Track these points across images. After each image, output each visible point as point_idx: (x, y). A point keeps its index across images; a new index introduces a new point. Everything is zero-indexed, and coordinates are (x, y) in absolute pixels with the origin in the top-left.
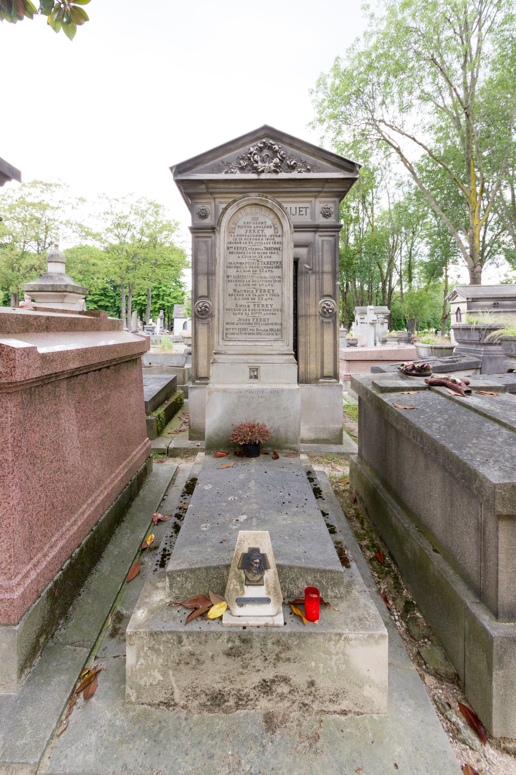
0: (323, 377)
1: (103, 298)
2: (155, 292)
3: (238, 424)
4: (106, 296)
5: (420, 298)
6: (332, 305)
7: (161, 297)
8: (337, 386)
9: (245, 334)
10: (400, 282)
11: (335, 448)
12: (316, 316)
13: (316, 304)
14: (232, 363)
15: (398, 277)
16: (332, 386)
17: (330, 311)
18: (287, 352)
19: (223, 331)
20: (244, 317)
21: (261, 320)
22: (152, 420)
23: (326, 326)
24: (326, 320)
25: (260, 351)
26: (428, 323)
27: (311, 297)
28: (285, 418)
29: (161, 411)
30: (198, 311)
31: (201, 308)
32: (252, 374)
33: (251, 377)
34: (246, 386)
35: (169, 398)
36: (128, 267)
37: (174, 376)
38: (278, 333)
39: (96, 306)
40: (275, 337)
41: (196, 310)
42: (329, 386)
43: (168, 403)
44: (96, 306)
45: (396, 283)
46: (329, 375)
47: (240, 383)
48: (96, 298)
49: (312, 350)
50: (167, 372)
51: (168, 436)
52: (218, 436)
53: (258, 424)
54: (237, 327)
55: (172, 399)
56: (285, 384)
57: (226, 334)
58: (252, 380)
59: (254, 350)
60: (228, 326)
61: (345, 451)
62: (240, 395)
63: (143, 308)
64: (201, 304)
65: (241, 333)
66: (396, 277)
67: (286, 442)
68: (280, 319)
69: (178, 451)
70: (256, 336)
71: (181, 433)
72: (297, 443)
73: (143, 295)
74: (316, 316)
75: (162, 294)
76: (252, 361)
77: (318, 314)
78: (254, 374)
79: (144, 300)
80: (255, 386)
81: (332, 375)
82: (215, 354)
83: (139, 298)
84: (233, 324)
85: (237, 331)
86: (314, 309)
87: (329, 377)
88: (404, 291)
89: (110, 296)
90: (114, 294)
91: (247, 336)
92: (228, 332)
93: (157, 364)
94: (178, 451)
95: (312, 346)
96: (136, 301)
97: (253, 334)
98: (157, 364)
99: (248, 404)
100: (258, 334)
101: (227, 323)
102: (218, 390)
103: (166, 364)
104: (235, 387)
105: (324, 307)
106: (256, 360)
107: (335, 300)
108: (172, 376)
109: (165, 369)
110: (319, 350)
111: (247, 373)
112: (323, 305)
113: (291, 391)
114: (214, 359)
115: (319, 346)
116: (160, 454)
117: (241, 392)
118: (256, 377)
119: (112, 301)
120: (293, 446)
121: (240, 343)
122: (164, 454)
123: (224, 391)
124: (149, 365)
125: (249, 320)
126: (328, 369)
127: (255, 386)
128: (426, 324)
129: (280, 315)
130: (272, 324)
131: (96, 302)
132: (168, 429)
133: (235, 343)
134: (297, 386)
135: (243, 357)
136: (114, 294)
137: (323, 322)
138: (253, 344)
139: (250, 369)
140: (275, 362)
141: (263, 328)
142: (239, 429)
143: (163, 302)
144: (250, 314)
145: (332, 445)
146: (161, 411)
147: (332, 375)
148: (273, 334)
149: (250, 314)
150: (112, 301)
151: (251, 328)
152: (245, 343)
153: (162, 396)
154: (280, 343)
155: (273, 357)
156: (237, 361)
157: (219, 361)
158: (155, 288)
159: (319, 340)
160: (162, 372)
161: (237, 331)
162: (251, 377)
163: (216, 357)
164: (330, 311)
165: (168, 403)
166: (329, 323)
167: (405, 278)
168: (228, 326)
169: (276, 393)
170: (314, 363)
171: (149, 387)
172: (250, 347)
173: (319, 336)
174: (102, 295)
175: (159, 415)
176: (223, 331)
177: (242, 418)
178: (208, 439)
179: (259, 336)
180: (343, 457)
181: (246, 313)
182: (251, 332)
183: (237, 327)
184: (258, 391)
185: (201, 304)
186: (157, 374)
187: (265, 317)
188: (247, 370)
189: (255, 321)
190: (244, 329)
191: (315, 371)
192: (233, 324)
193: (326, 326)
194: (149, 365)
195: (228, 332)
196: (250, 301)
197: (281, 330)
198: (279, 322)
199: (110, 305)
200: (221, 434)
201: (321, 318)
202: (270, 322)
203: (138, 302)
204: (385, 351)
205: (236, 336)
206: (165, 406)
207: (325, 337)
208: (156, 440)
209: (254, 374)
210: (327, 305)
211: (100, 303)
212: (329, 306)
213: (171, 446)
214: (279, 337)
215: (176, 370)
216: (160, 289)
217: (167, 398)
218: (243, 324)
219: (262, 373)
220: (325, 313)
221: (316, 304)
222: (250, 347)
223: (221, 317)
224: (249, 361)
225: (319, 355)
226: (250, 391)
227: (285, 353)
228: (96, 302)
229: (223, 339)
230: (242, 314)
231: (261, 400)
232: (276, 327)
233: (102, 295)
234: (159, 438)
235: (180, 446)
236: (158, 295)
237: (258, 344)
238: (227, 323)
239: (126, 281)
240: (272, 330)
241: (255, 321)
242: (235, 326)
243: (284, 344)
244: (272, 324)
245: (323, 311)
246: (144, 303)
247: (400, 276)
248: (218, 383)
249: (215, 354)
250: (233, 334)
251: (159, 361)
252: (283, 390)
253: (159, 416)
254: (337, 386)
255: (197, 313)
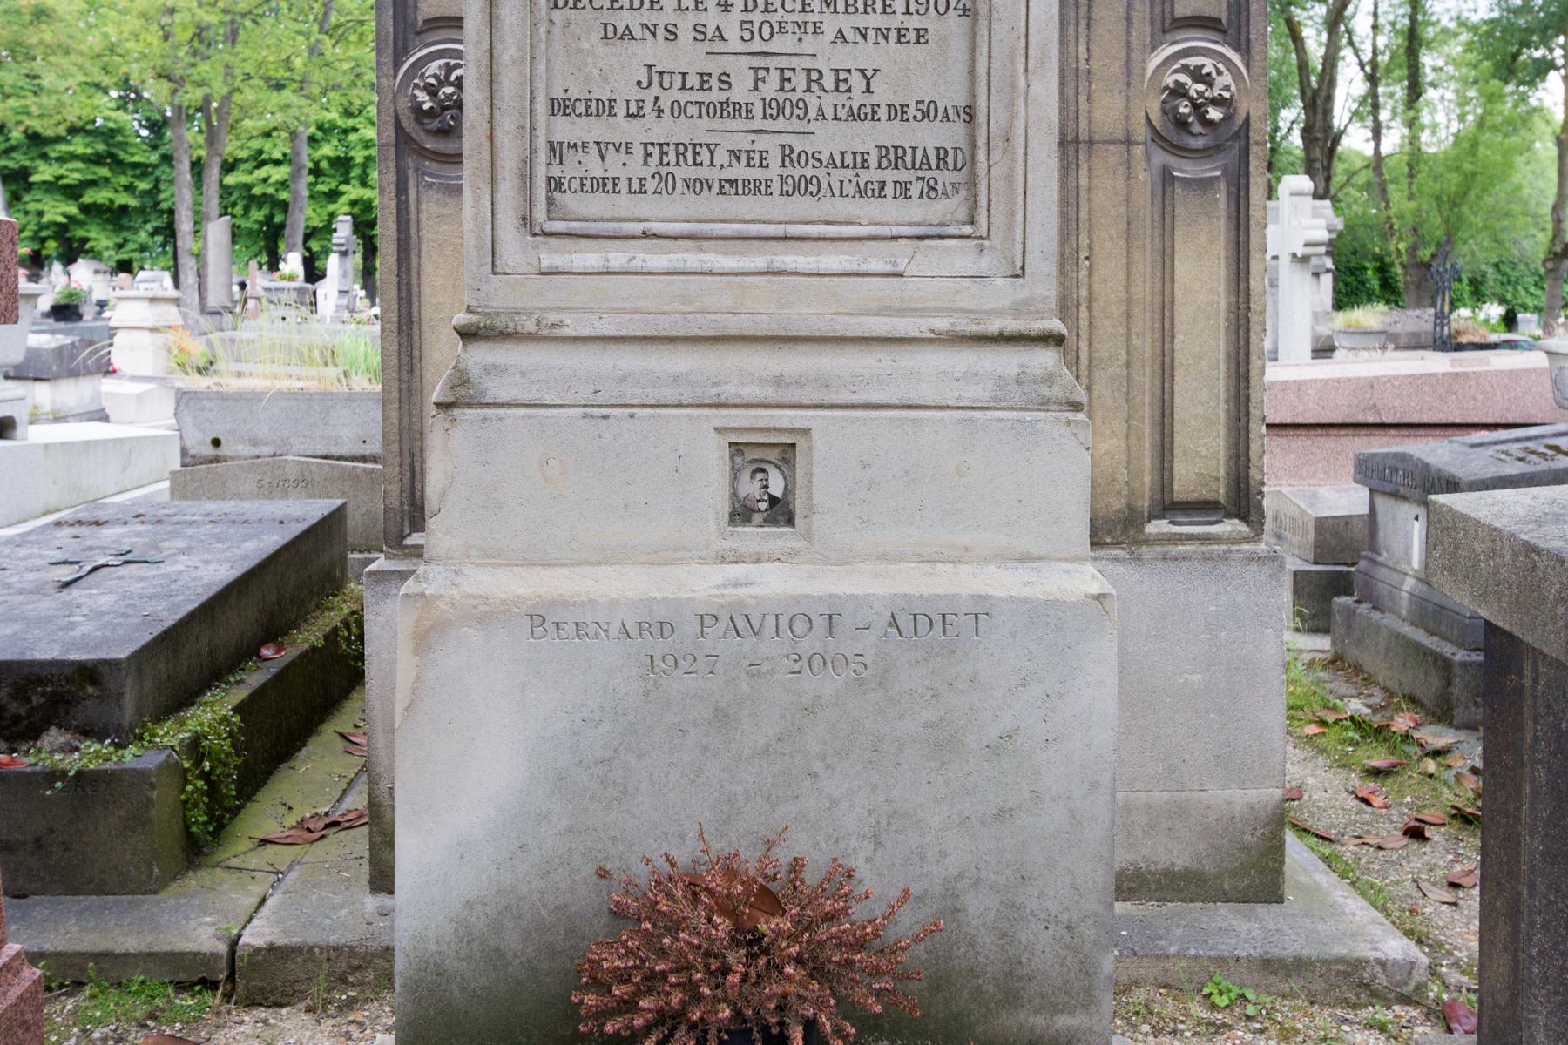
0: (1169, 507)
1: (104, 172)
2: (327, 150)
3: (642, 874)
4: (118, 164)
5: (1467, 167)
6: (1227, 79)
7: (355, 172)
8: (1253, 558)
9: (697, 186)
10: (1372, 103)
11: (1242, 930)
12: (1129, 142)
13: (1129, 70)
14: (597, 408)
15: (1360, 87)
16: (1224, 557)
17: (1214, 114)
18: (1012, 325)
19: (528, 162)
20: (687, 56)
21: (814, 79)
22: (140, 775)
23: (1185, 204)
24: (1186, 169)
25: (806, 313)
26: (1472, 282)
27: (1099, 30)
28: (1003, 814)
29: (213, 713)
30: (417, 109)
31: (432, 91)
32: (750, 488)
33: (741, 513)
34: (704, 584)
35: (293, 625)
36: (200, 33)
37: (339, 502)
38: (945, 177)
39: (73, 210)
40: (918, 210)
41: (404, 104)
42: (1206, 559)
43: (275, 658)
44: (73, 210)
45: (1347, 116)
46: (1204, 493)
47: (658, 557)
48: (73, 174)
49: (1103, 349)
50: (305, 484)
51: (253, 861)
52: (496, 957)
53: (797, 865)
54: (635, 132)
55: (308, 637)
56: (1002, 558)
57: (554, 185)
58: (754, 536)
59: (763, 308)
60: (566, 129)
61: (1309, 952)
62: (660, 647)
63: (278, 219)
64: (434, 67)
65: (666, 182)
66: (1349, 85)
67: (1011, 997)
68: (958, 71)
69: (294, 968)
70: (773, 210)
71: (334, 837)
72: (1087, 1001)
73: (277, 163)
74: (1129, 142)
75: (359, 156)
76: (749, 392)
77: (1141, 132)
78: (767, 495)
79: (283, 184)
80: (774, 575)
81: (1221, 494)
82: (468, 335)
83: (262, 173)
84: (605, 108)
85: (636, 168)
86: (1118, 103)
87: (1205, 508)
88: (1386, 148)
89: (135, 165)
90: (154, 158)
91: (711, 203)
92: (570, 170)
93: (255, 443)
94: (294, 968)
95: (1105, 326)
96: (248, 187)
97: (758, 188)
98: (255, 443)
99: (723, 718)
100: (792, 188)
101: (560, 107)
102: (488, 615)
103: (299, 445)
104: (621, 586)
105: (1178, 92)
106: (778, 381)
107: (1243, 47)
108: (314, 509)
109: (292, 473)
110: (1146, 345)
111: (713, 484)
112: (1169, 80)
113: (1043, 615)
114: (461, 379)
115: (1144, 321)
116: (181, 987)
117: (665, 628)
118: (780, 511)
119: (143, 185)
120: (1063, 1022)
121: (659, 258)
122: (210, 985)
123: (537, 620)
124: (208, 451)
125: (725, 81)
126: (1200, 462)
127: (774, 575)
128: (1466, 288)
129: (958, 48)
130: (898, 112)
131: (72, 192)
132: (266, 815)
133: (617, 257)
134: (1085, 578)
135: (682, 361)
136: (154, 158)
137: (1167, 178)
138: (758, 261)
139: (737, 448)
140: (927, 394)
141: (829, 139)
142: (644, 914)
143: (366, 194)
144: (732, 33)
145: (1223, 909)
146: (213, 713)
147: (1221, 494)
148: (903, 189)
149: (732, 33)
150: (143, 185)
151: (742, 142)
152: (691, 258)
153: (239, 623)
154: (960, 257)
155: (908, 359)
156: (634, 394)
157: (497, 390)
158: (325, 129)
159: (1145, 289)
160: (277, 487)
161: (636, 168)
162: (741, 513)
163: (479, 356)
164: (1214, 114)
165: (275, 658)
166: (1204, 185)
167: (1393, 91)
168: (566, 129)
169: (933, 627)
170: (1118, 425)
171: (166, 569)
172: (726, 282)
173: (1145, 263)
174: (97, 159)
175: (197, 739)
176: (528, 162)
177: (674, 821)
178: (414, 986)
179: (801, 205)
180: (1295, 984)
181: (699, 31)
182: (739, 171)
183: (635, 132)
184: (793, 618)
185: (434, 67)
186: (253, 496)
187: (844, 57)
188: (715, 456)
189: (770, 88)
190: (689, 152)
191: (1123, 475)
192: (605, 108)
193: (1185, 204)
194: (208, 451)
195: (570, 170)
196: (734, 44)
197: (965, 161)
198: (952, 95)
199: (133, 202)
200: (512, 941)
201: (1160, 157)
202: (883, 94)
203: (257, 191)
204: (1390, 379)
205: (624, 204)
206: (255, 678)
207: (1183, 269)
208: (168, 896)
209: (767, 495)
210: (1198, 75)
211: (89, 197)
212: (1207, 80)
213: (254, 937)
214: (948, 208)
215: (355, 478)
216: (352, 137)
217: (275, 632)
218: (679, 110)
219: (824, 479)
220: (1181, 124)
221: (1129, 70)
222: (726, 282)
223: (509, 52)
224: (730, 391)
225: (1146, 379)
226: (739, 621)
227: (994, 326)
228: (72, 192)
229: (526, 221)
230: (672, 34)
231: (827, 685)
232: (930, 137)
233: (97, 159)
234: (193, 881)
235: (312, 937)
236: (342, 164)
237: (790, 258)
238: (560, 107)
239: (193, 96)
240: (894, 157)
241: (770, 88)
242: (620, 128)
243: (985, 263)
244: (898, 112)
245: (1169, 112)
246: (284, 195)
247: (1372, 79)
248: (491, 557)
249: (468, 335)
250: (602, 185)
251: (263, 431)
252: (981, 612)
253: (195, 747)
254: (1253, 558)
255: (409, 124)
